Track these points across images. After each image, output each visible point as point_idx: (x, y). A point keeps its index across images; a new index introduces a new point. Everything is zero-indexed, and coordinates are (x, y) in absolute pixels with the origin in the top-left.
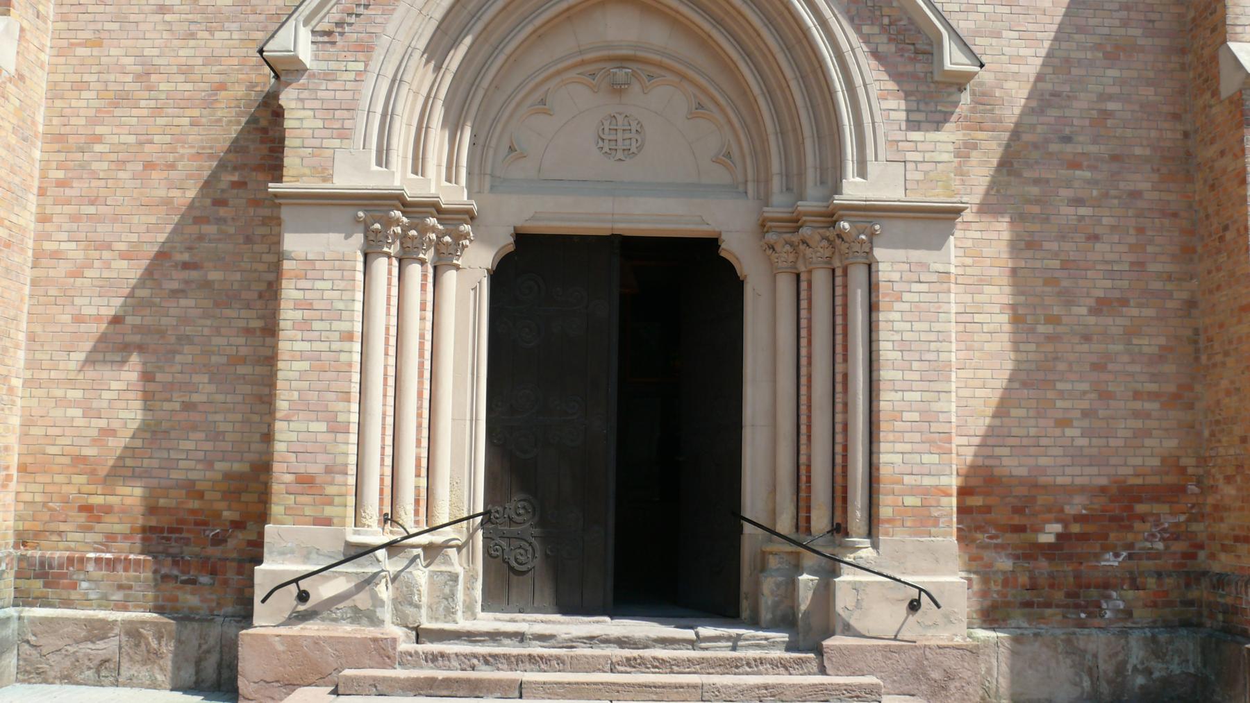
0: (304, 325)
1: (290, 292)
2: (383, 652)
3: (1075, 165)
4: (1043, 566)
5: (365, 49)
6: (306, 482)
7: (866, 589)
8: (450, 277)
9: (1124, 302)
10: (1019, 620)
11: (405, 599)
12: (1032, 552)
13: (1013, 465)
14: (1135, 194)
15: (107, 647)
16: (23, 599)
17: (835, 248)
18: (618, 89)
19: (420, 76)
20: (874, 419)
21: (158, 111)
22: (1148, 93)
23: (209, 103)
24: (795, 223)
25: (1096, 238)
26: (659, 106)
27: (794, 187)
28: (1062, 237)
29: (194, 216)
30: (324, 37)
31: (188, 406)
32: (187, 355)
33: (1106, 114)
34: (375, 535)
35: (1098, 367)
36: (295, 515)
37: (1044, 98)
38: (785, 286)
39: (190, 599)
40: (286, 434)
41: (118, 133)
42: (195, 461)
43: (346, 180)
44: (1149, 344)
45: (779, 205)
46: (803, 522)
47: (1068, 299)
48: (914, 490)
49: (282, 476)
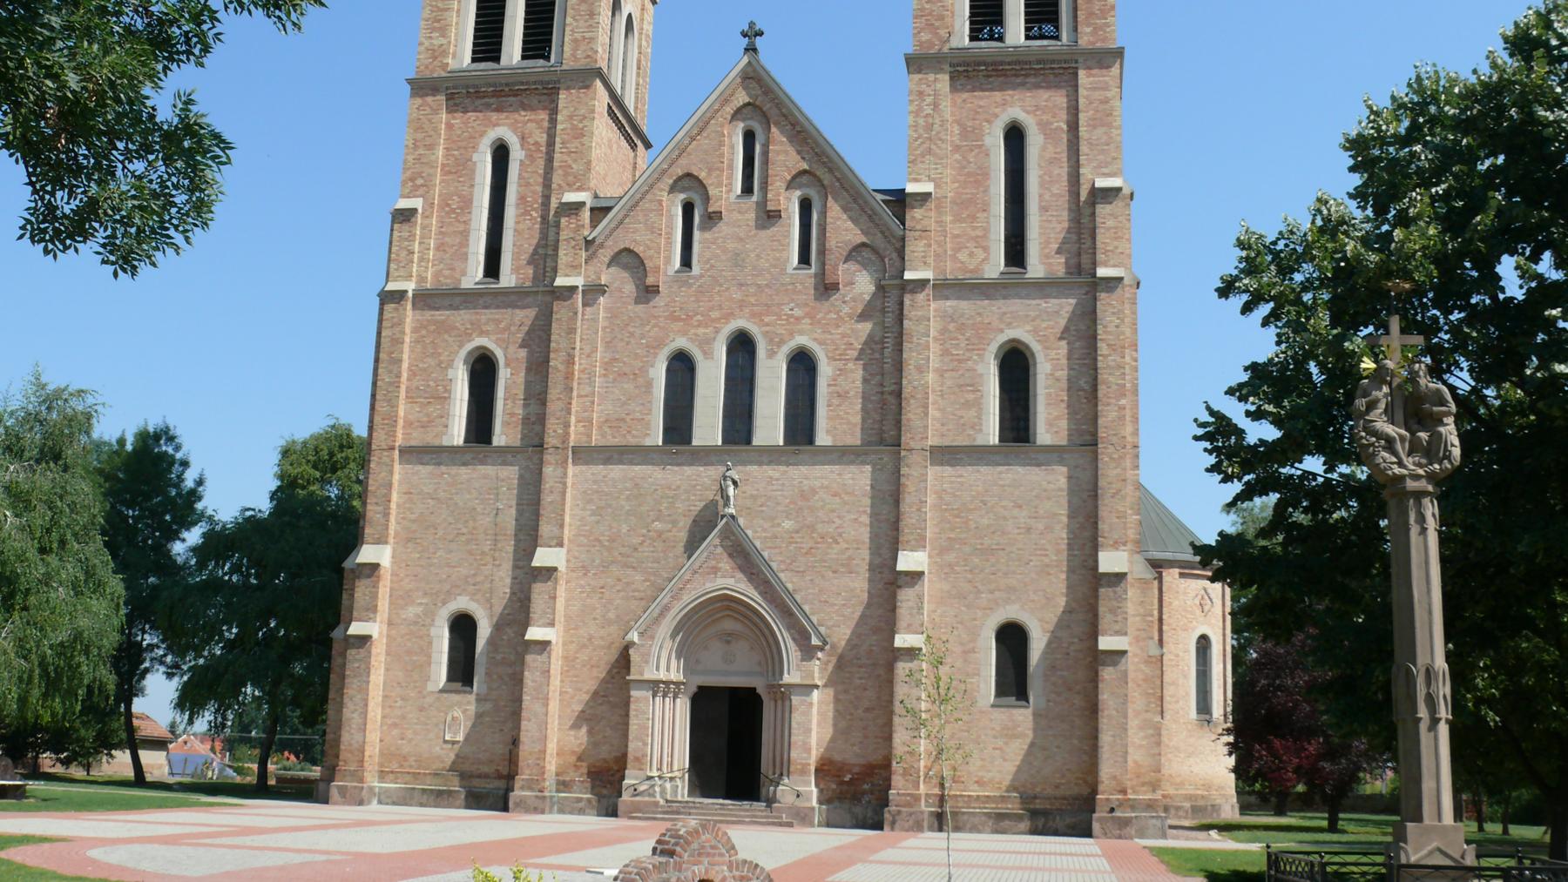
1: (632, 706)
2: (656, 804)
4: (845, 787)
5: (652, 638)
6: (637, 759)
7: (785, 791)
10: (837, 804)
11: (663, 791)
12: (843, 783)
13: (837, 757)
15: (581, 805)
16: (558, 791)
17: (783, 695)
18: (728, 642)
19: (668, 644)
23: (609, 647)
29: (604, 681)
30: (641, 634)
34: (655, 773)
37: (852, 644)
39: (605, 792)
40: (631, 746)
41: (583, 657)
42: (606, 753)
43: (648, 676)
49: (630, 756)
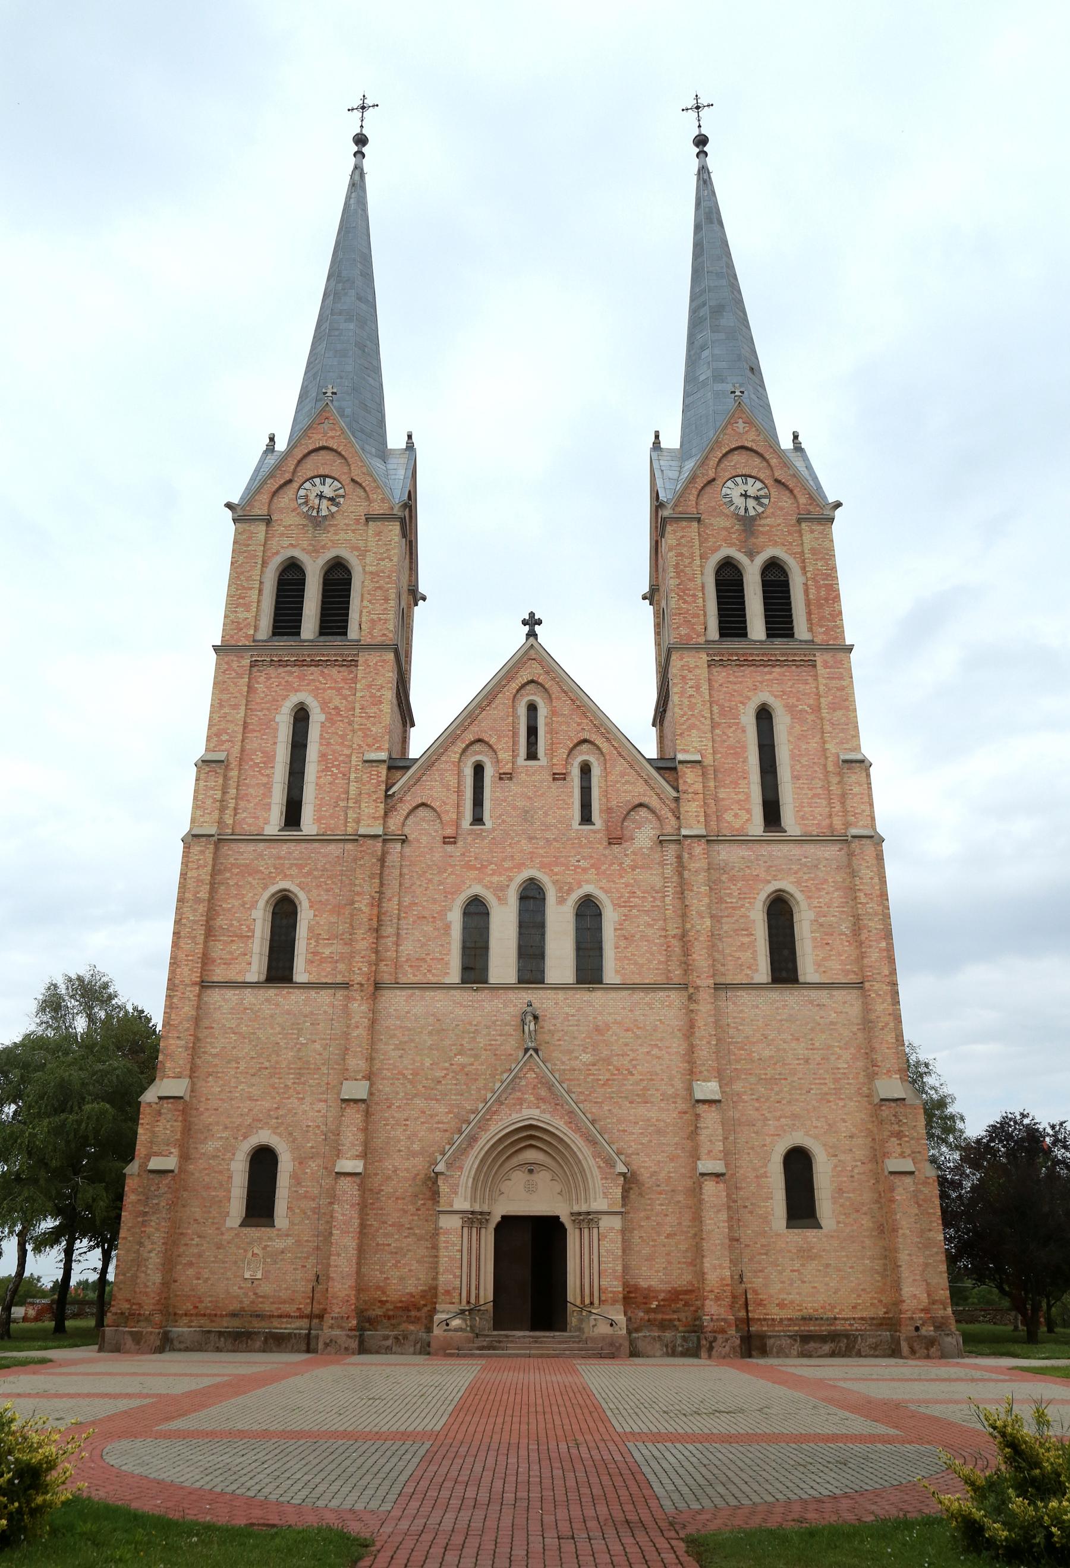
5: (461, 1168)
8: (483, 1231)
9: (675, 1234)
15: (389, 1342)
20: (32, 1367)
23: (414, 1178)
25: (667, 1215)
31: (410, 1270)
33: (670, 1177)
35: (668, 1254)
40: (442, 1279)
46: (583, 1301)
48: (611, 1292)
49: (441, 1290)
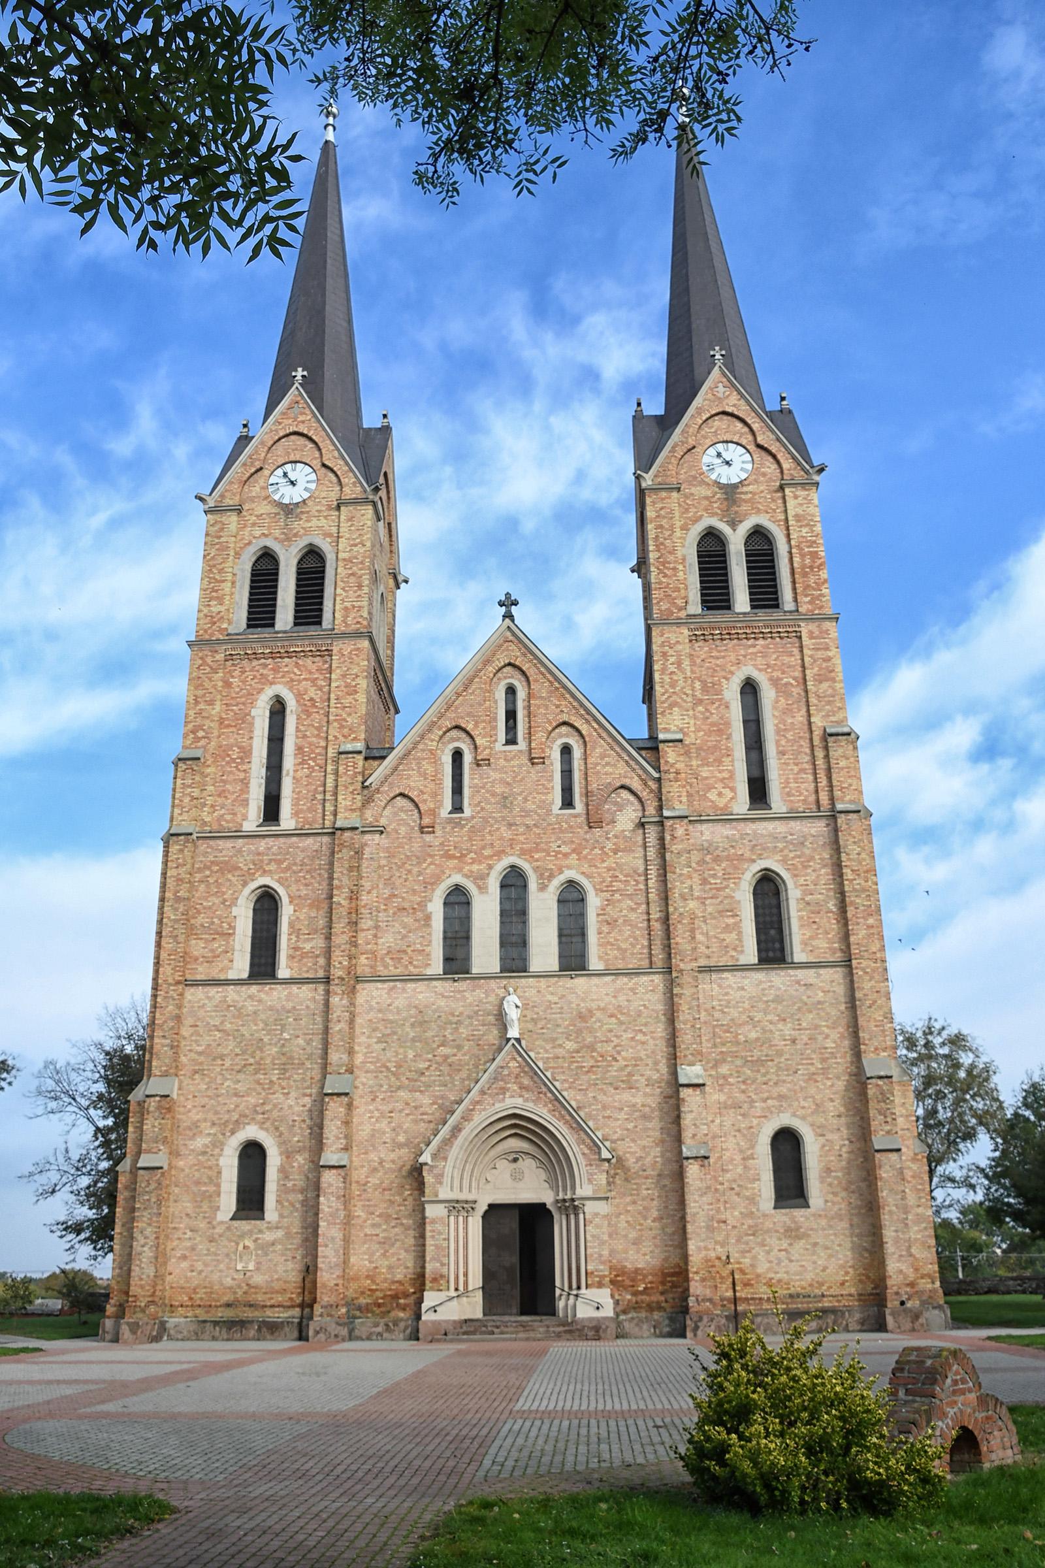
0: (433, 1237)
3: (647, 1178)
5: (445, 1159)
14: (665, 1186)
21: (386, 1173)
22: (668, 1154)
24: (564, 1200)
26: (527, 1164)
27: (565, 1190)
28: (643, 1200)
31: (399, 1260)
32: (398, 1244)
36: (432, 1289)
38: (564, 1217)
44: (669, 1230)
45: (561, 1196)
47: (645, 1219)
